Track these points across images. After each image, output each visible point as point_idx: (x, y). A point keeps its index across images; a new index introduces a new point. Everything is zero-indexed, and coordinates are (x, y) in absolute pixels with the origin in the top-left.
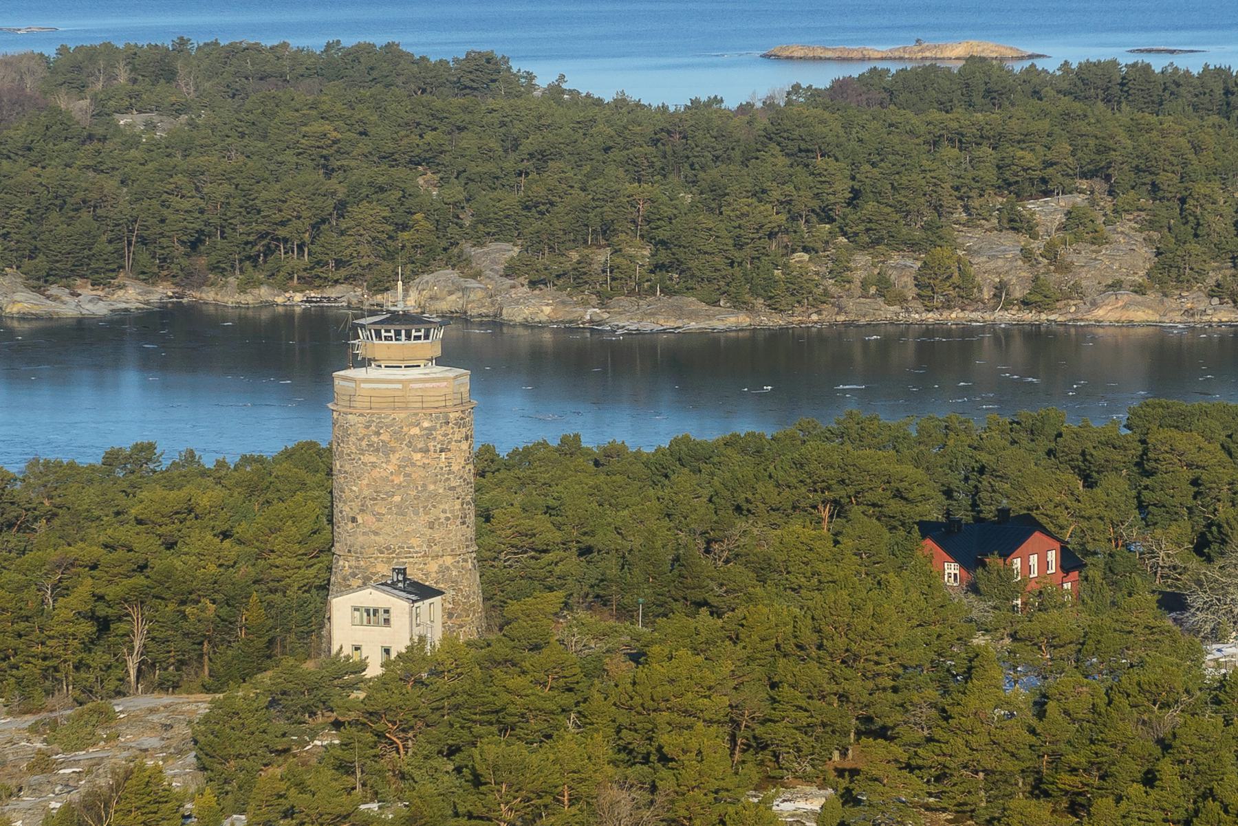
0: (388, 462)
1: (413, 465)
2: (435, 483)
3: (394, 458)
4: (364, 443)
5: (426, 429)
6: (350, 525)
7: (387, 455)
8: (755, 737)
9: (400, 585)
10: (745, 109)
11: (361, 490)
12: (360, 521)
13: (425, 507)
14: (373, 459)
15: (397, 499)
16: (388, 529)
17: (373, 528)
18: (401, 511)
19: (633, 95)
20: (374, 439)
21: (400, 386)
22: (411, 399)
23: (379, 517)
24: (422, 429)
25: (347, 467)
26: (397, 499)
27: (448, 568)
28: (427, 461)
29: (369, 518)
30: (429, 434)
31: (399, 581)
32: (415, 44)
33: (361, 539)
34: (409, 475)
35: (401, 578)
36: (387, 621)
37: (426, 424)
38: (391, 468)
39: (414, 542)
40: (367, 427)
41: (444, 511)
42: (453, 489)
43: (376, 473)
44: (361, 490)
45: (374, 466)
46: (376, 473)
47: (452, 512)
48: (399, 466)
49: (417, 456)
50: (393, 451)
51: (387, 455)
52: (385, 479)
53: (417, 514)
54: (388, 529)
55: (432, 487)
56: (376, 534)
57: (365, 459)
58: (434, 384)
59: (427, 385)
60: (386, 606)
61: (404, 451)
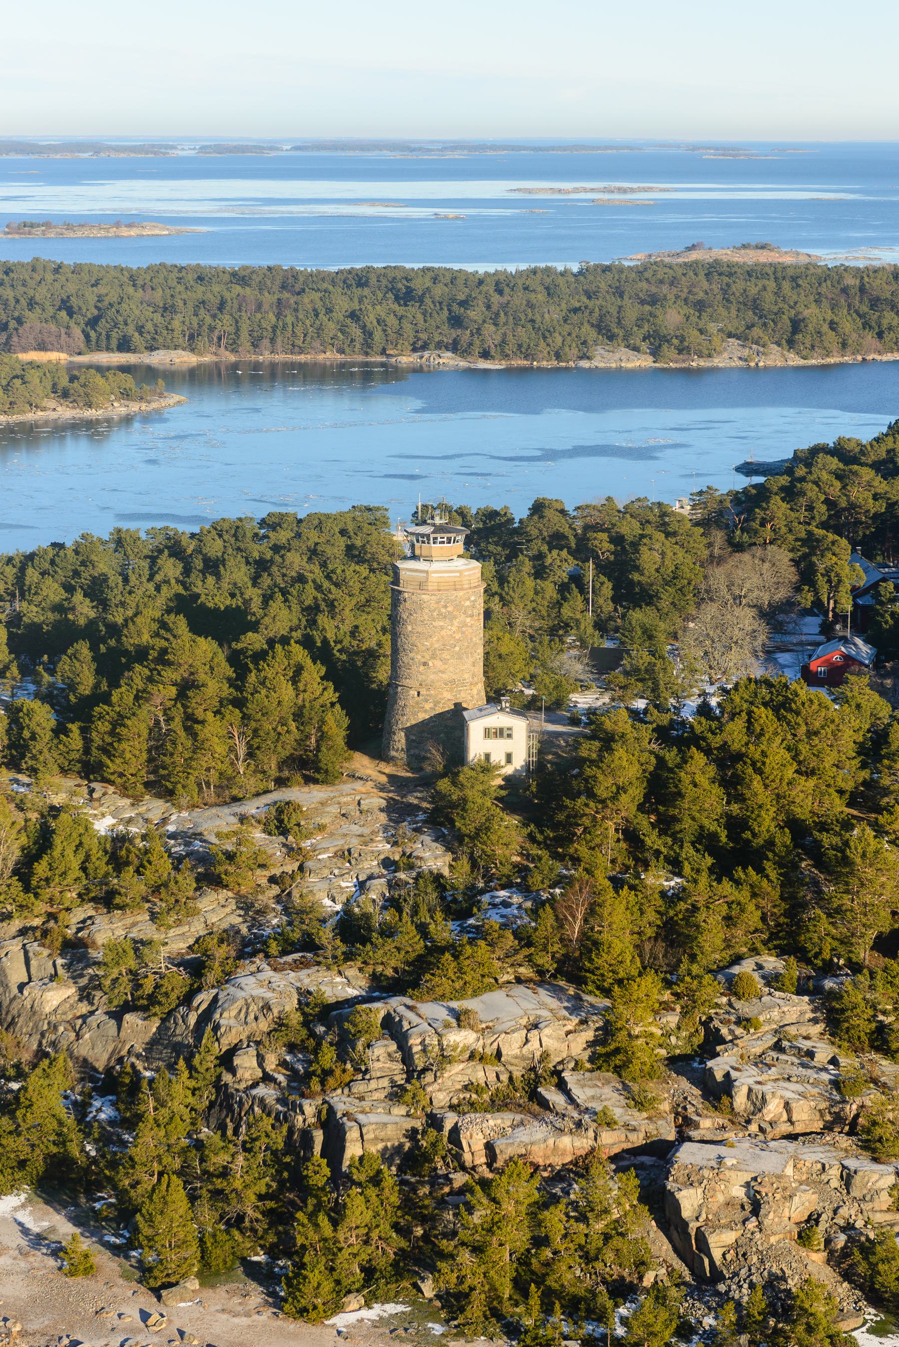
3: (456, 623)
6: (422, 668)
7: (451, 620)
8: (695, 909)
11: (432, 645)
14: (442, 623)
15: (457, 649)
16: (451, 669)
20: (443, 610)
23: (445, 661)
25: (420, 629)
32: (375, 265)
33: (432, 677)
36: (509, 736)
37: (473, 598)
38: (454, 629)
39: (466, 676)
44: (432, 645)
45: (442, 628)
46: (443, 633)
49: (468, 620)
54: (451, 669)
56: (443, 672)
57: (436, 624)
60: (509, 725)
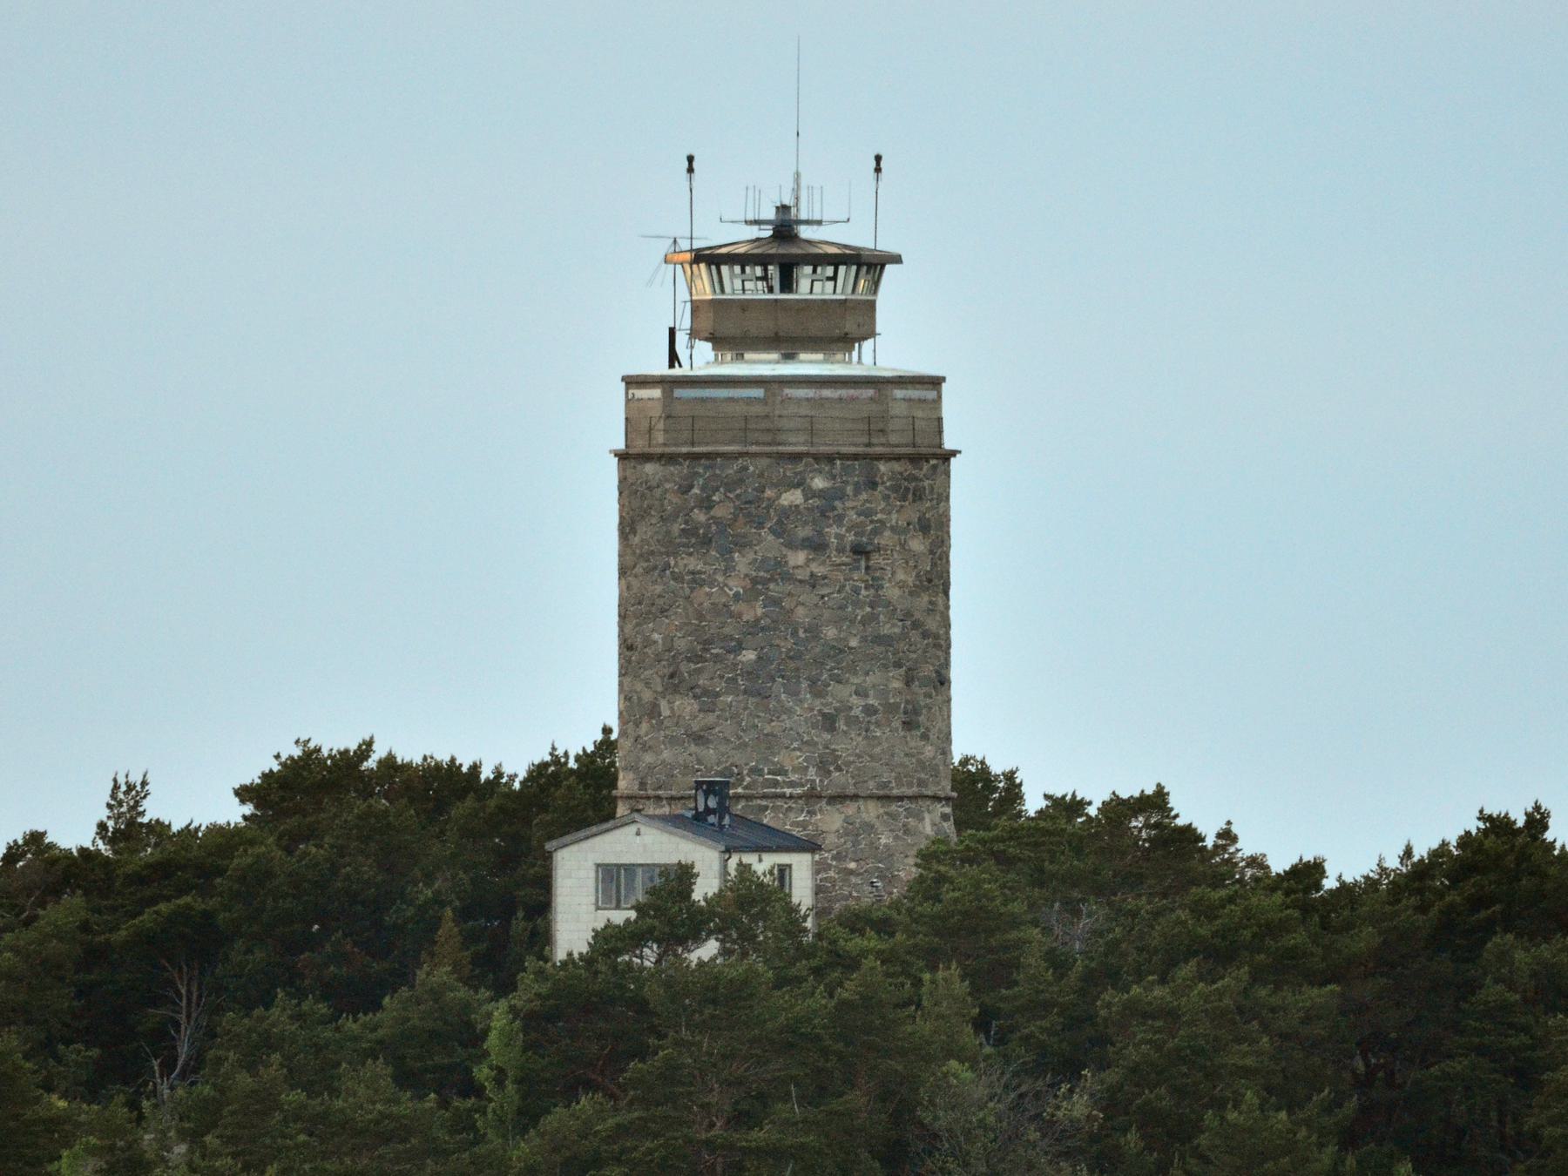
0: (728, 570)
1: (788, 577)
2: (837, 622)
4: (676, 528)
5: (821, 494)
7: (726, 554)
9: (712, 819)
10: (1256, 862)
12: (666, 712)
13: (813, 682)
14: (694, 564)
15: (749, 656)
17: (695, 727)
18: (756, 684)
19: (1197, 810)
20: (700, 516)
21: (758, 393)
22: (785, 424)
23: (707, 700)
24: (809, 494)
26: (749, 656)
27: (869, 828)
28: (819, 570)
29: (686, 706)
30: (826, 506)
31: (708, 811)
34: (776, 602)
35: (712, 803)
40: (685, 490)
41: (861, 692)
42: (879, 640)
43: (704, 596)
45: (697, 580)
47: (883, 693)
48: (755, 581)
49: (798, 558)
50: (742, 544)
51: (726, 554)
52: (722, 610)
53: (794, 694)
55: (830, 632)
58: (852, 392)
59: (827, 393)
61: (769, 544)
